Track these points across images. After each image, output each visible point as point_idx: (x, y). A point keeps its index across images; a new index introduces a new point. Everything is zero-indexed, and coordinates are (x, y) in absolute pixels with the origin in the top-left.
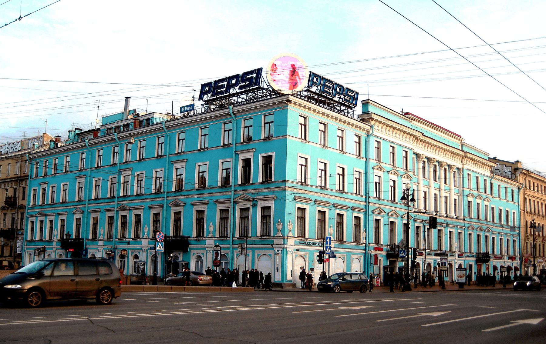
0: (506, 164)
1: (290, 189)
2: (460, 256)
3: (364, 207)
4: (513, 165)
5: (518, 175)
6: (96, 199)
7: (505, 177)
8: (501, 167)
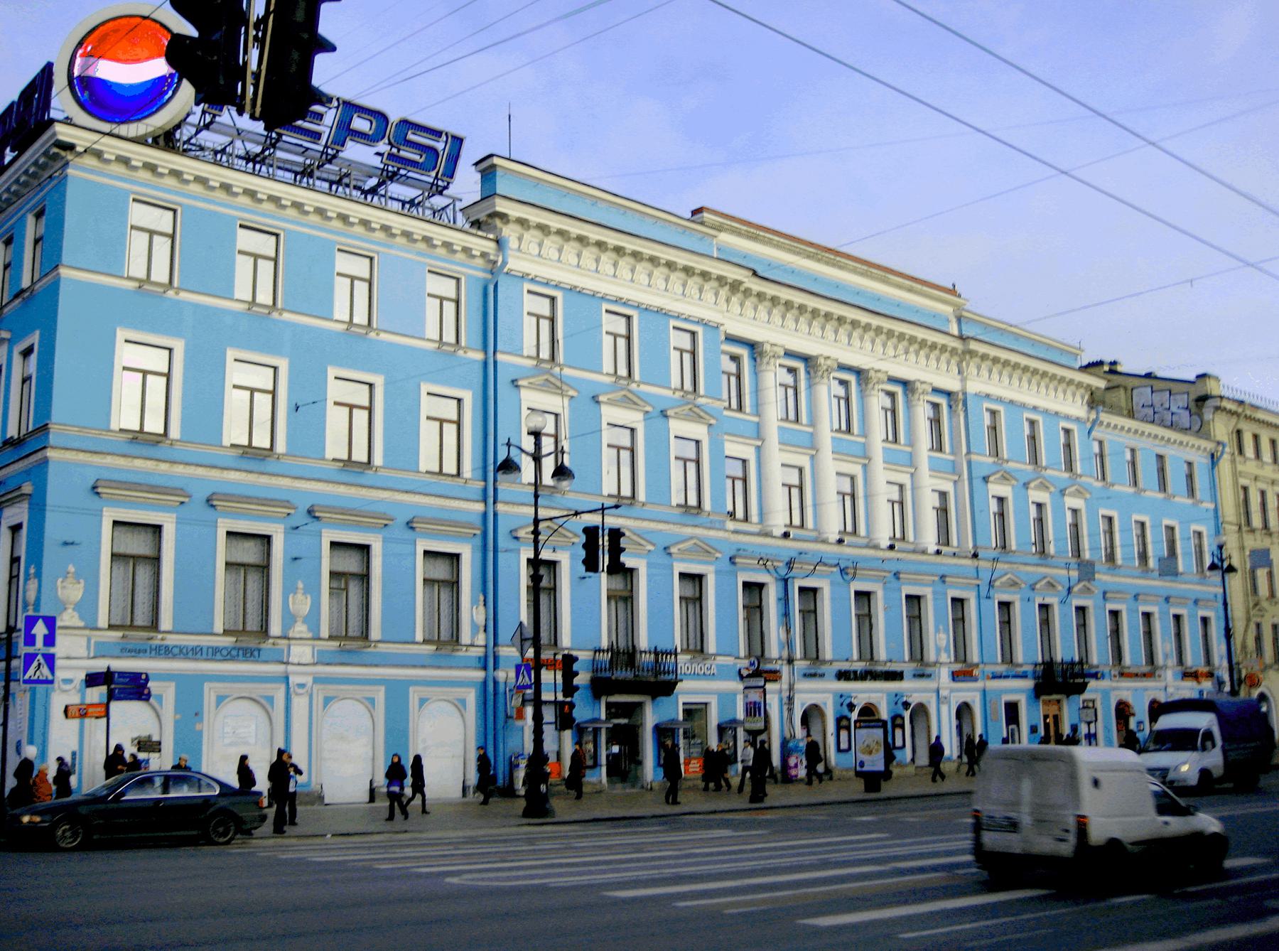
1: (470, 497)
2: (963, 674)
3: (478, 521)
4: (1192, 388)
5: (1208, 415)
7: (1171, 426)
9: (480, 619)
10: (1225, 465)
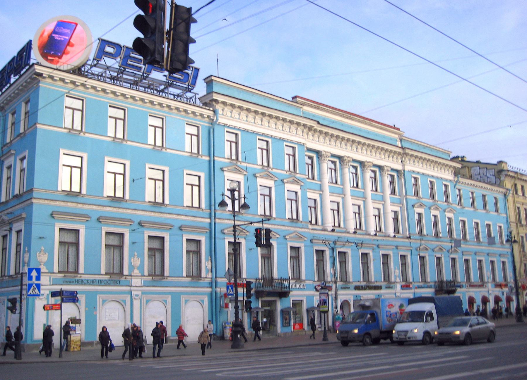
0: (488, 167)
2: (406, 286)
3: (207, 226)
5: (503, 178)
8: (481, 171)
9: (209, 266)
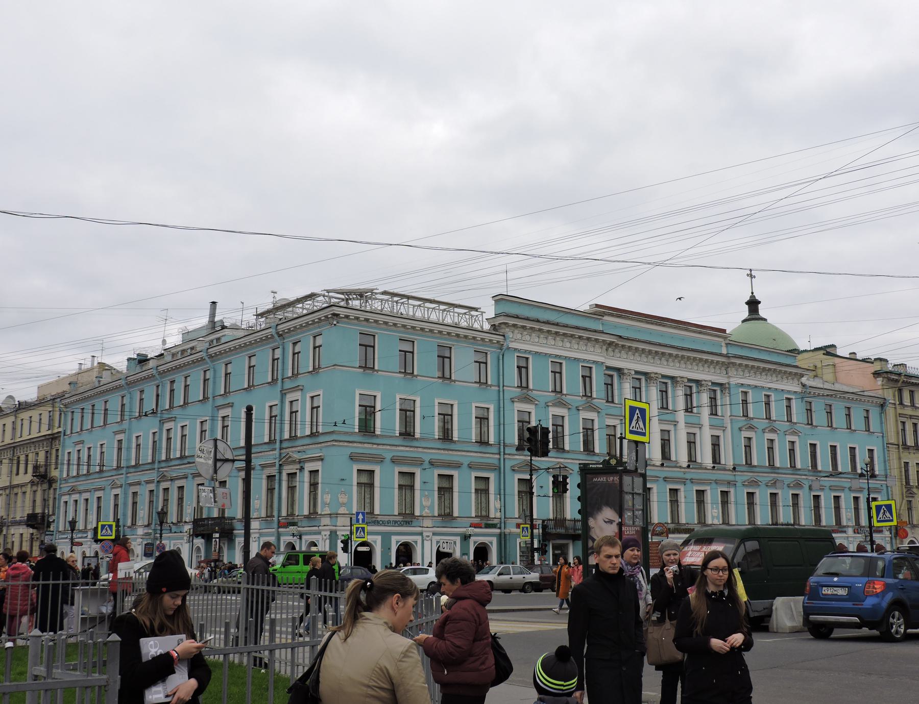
6: (137, 465)
9: (498, 506)
10: (890, 411)
